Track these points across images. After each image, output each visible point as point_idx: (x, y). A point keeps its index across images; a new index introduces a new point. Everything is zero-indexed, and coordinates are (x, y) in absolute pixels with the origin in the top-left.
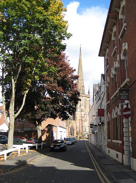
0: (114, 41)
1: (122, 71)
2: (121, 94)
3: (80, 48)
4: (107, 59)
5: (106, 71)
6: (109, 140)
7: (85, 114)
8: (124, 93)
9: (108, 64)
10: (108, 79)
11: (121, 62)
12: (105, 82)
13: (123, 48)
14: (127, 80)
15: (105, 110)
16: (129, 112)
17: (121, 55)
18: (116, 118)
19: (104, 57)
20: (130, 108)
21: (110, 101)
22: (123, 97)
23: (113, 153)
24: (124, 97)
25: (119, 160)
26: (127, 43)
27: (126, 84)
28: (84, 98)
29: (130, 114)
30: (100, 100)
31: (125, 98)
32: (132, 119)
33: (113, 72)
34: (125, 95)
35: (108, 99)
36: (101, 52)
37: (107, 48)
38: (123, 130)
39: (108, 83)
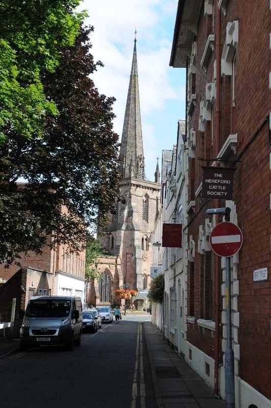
0: (210, 16)
1: (223, 112)
2: (209, 181)
3: (135, 41)
4: (194, 75)
5: (188, 112)
6: (191, 319)
7: (145, 237)
8: (218, 178)
9: (194, 86)
10: (193, 134)
11: (224, 82)
12: (187, 143)
13: (228, 40)
14: (233, 138)
15: (183, 227)
16: (235, 239)
17: (223, 61)
18: (208, 254)
19: (186, 68)
20: (237, 225)
21: (196, 203)
22: (214, 190)
23: (199, 359)
24: (218, 190)
25: (210, 380)
26: (236, 23)
27: (229, 151)
28: (141, 192)
29: (238, 244)
30: (174, 197)
31: (219, 194)
32: (240, 258)
33: (205, 114)
34: (219, 184)
35: (192, 197)
36: (186, 9)
37: (194, 41)
38: (220, 289)
39: (193, 148)
